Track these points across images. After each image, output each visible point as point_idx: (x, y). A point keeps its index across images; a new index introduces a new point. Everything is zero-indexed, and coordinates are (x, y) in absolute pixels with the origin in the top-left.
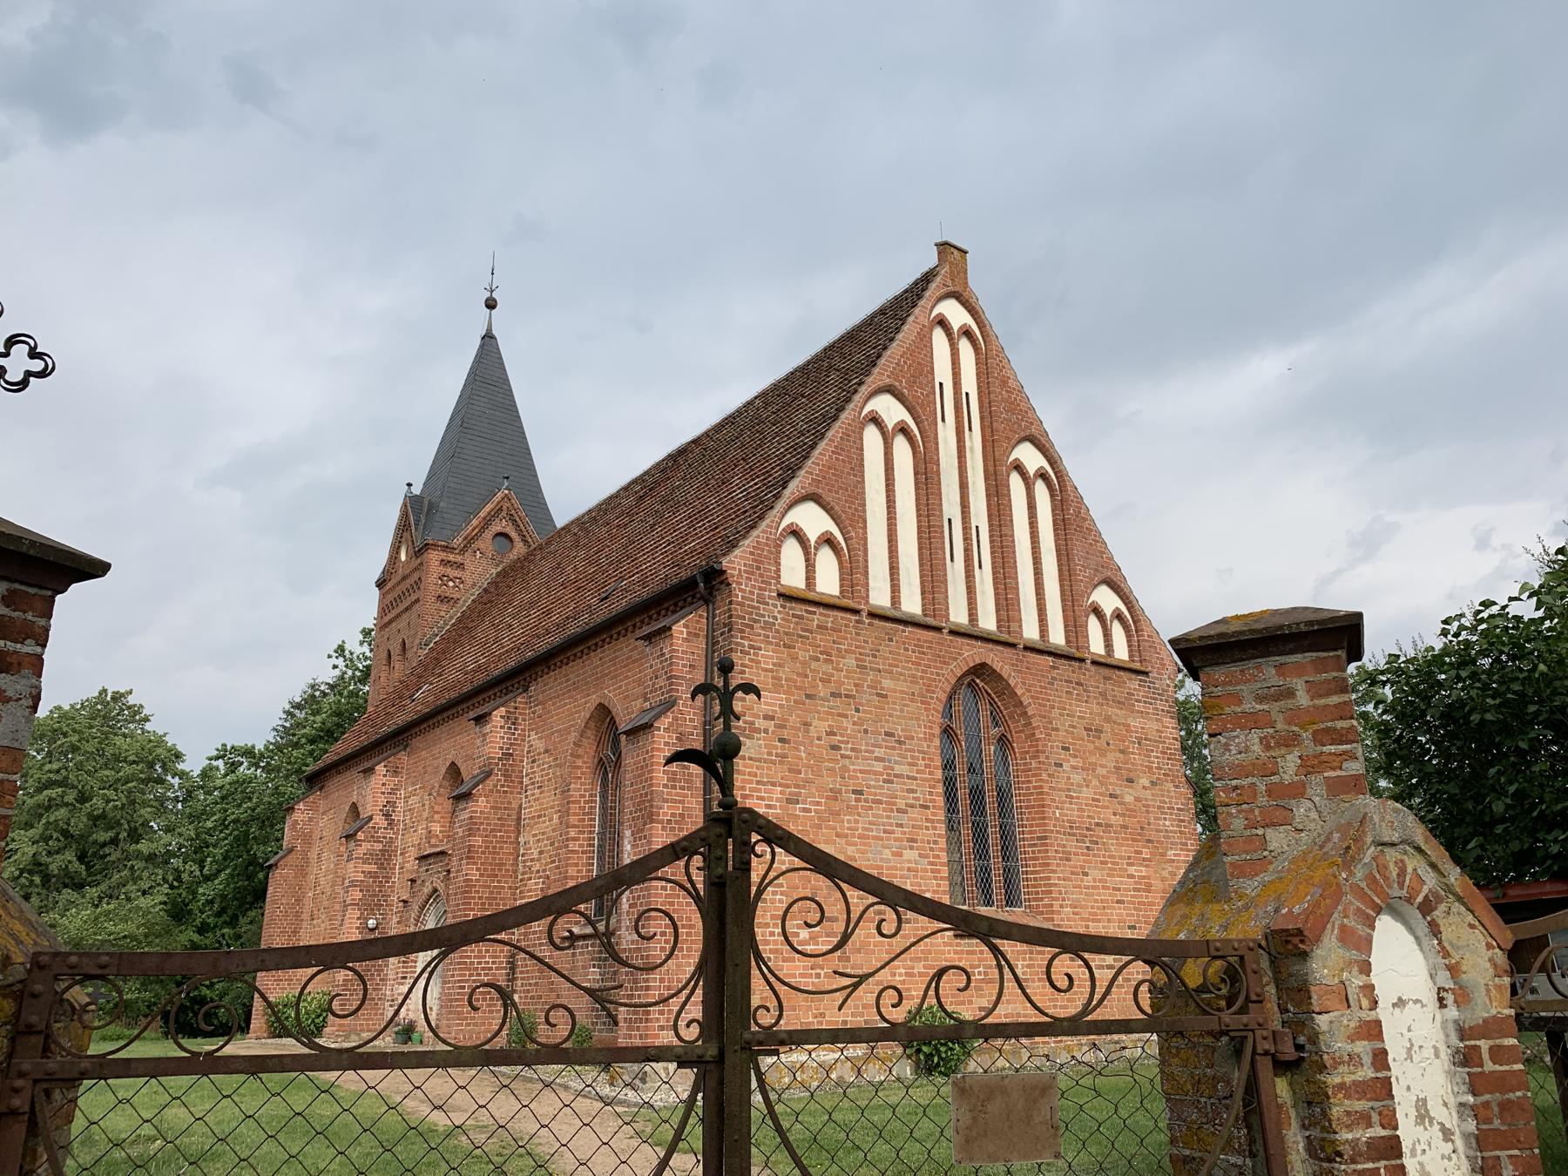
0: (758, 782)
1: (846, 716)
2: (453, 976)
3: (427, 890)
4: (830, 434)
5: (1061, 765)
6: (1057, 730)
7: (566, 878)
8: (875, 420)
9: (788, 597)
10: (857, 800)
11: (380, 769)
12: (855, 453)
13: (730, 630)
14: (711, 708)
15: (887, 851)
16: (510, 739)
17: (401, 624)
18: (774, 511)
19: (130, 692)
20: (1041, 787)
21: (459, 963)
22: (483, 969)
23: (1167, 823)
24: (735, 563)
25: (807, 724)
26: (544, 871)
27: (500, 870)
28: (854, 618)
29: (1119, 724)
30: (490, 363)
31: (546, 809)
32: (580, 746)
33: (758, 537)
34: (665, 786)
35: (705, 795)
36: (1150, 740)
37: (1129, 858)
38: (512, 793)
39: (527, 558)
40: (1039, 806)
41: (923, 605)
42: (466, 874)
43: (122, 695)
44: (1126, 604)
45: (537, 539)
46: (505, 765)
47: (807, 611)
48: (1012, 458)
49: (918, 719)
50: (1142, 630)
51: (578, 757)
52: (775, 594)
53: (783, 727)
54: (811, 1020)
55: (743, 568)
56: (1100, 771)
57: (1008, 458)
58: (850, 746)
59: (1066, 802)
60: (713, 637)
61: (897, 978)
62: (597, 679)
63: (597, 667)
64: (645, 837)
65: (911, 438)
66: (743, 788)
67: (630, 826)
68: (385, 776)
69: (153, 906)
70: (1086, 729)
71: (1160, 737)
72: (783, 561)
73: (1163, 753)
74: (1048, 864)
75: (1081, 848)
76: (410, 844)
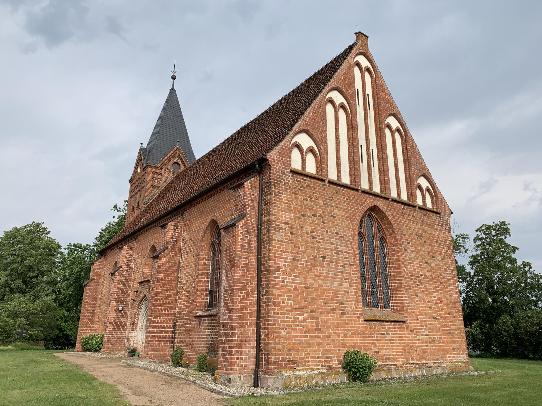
0: (282, 251)
1: (318, 225)
2: (150, 331)
3: (142, 295)
4: (313, 105)
5: (407, 250)
6: (405, 235)
7: (197, 291)
8: (331, 101)
9: (294, 172)
10: (323, 261)
11: (125, 248)
12: (323, 114)
13: (270, 185)
14: (261, 219)
15: (336, 283)
16: (175, 234)
17: (138, 196)
18: (289, 136)
19: (43, 223)
20: (399, 258)
21: (152, 326)
22: (162, 328)
23: (448, 275)
24: (272, 156)
25: (302, 227)
26: (188, 288)
27: (170, 288)
28: (322, 183)
29: (429, 234)
30: (173, 99)
31: (189, 263)
32: (204, 237)
33: (282, 146)
34: (241, 251)
35: (258, 256)
36: (441, 241)
37: (434, 289)
38: (176, 256)
39: (185, 171)
40: (398, 267)
41: (350, 180)
42: (156, 289)
43: (40, 224)
44: (431, 185)
45: (189, 164)
46: (173, 245)
47: (302, 179)
48: (386, 122)
49: (349, 228)
50: (438, 196)
51: (203, 241)
52: (289, 171)
53: (292, 228)
54: (304, 356)
55: (275, 159)
56: (422, 253)
57: (385, 121)
58: (320, 237)
59: (408, 265)
60: (262, 188)
61: (341, 338)
62: (211, 209)
63: (211, 204)
64: (232, 273)
65: (346, 110)
66: (275, 253)
67: (225, 269)
68: (127, 250)
69: (50, 300)
70: (417, 235)
71: (445, 240)
72: (292, 157)
73: (446, 246)
74: (402, 291)
75: (415, 284)
76: (136, 277)
